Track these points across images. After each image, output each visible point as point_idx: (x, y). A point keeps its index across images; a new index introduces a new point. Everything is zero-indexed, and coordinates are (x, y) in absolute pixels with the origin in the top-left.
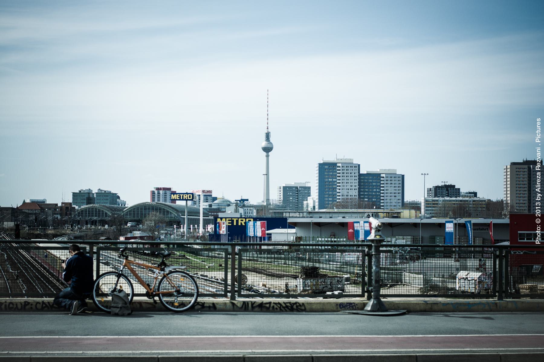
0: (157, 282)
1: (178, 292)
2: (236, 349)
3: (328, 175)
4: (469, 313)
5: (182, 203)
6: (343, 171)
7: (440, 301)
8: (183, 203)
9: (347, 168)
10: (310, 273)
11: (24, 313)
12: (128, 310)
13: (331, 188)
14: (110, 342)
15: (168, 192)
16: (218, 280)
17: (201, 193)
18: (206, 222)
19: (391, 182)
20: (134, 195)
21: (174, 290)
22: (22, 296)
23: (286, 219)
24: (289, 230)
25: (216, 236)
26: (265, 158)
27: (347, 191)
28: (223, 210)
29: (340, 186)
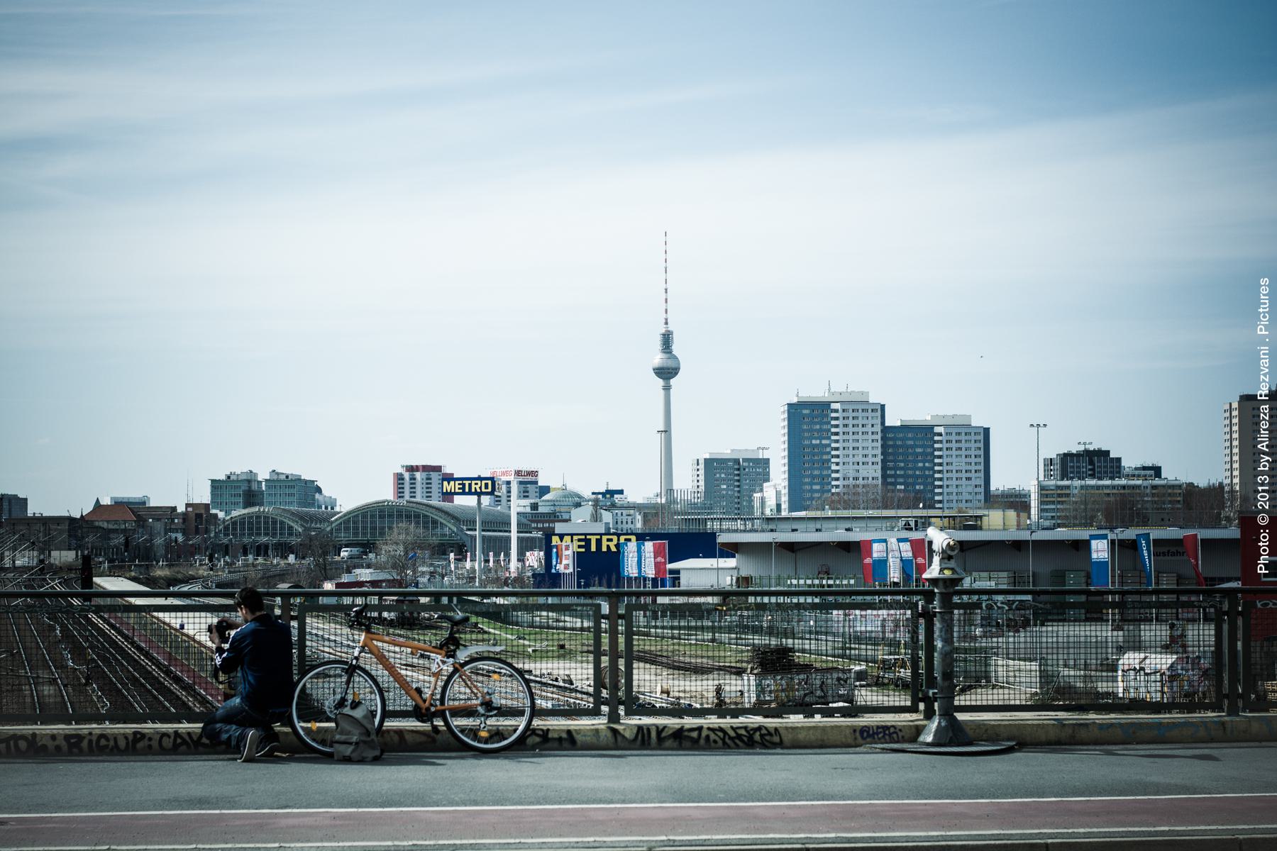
0: (440, 684)
1: (488, 705)
2: (631, 834)
3: (808, 431)
4: (1168, 746)
5: (465, 502)
6: (846, 422)
7: (1078, 719)
8: (471, 501)
9: (855, 414)
10: (773, 662)
11: (133, 758)
12: (373, 748)
13: (818, 461)
14: (338, 822)
15: (434, 475)
16: (556, 680)
17: (511, 478)
18: (525, 545)
19: (958, 445)
20: (354, 485)
21: (478, 702)
22: (99, 719)
23: (713, 535)
24: (721, 560)
25: (548, 577)
26: (662, 392)
27: (856, 467)
28: (565, 516)
29: (838, 456)
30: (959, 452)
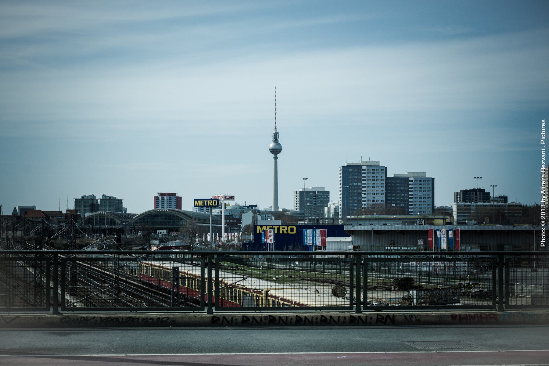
3: (352, 179)
6: (369, 175)
9: (373, 171)
13: (356, 193)
19: (420, 186)
26: (273, 160)
27: (373, 195)
29: (365, 191)
30: (420, 189)
